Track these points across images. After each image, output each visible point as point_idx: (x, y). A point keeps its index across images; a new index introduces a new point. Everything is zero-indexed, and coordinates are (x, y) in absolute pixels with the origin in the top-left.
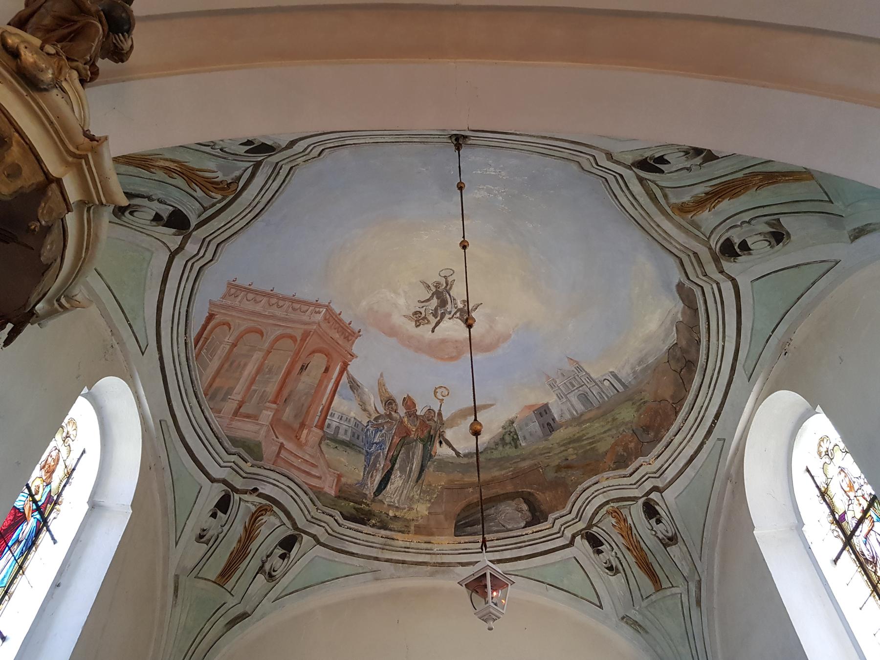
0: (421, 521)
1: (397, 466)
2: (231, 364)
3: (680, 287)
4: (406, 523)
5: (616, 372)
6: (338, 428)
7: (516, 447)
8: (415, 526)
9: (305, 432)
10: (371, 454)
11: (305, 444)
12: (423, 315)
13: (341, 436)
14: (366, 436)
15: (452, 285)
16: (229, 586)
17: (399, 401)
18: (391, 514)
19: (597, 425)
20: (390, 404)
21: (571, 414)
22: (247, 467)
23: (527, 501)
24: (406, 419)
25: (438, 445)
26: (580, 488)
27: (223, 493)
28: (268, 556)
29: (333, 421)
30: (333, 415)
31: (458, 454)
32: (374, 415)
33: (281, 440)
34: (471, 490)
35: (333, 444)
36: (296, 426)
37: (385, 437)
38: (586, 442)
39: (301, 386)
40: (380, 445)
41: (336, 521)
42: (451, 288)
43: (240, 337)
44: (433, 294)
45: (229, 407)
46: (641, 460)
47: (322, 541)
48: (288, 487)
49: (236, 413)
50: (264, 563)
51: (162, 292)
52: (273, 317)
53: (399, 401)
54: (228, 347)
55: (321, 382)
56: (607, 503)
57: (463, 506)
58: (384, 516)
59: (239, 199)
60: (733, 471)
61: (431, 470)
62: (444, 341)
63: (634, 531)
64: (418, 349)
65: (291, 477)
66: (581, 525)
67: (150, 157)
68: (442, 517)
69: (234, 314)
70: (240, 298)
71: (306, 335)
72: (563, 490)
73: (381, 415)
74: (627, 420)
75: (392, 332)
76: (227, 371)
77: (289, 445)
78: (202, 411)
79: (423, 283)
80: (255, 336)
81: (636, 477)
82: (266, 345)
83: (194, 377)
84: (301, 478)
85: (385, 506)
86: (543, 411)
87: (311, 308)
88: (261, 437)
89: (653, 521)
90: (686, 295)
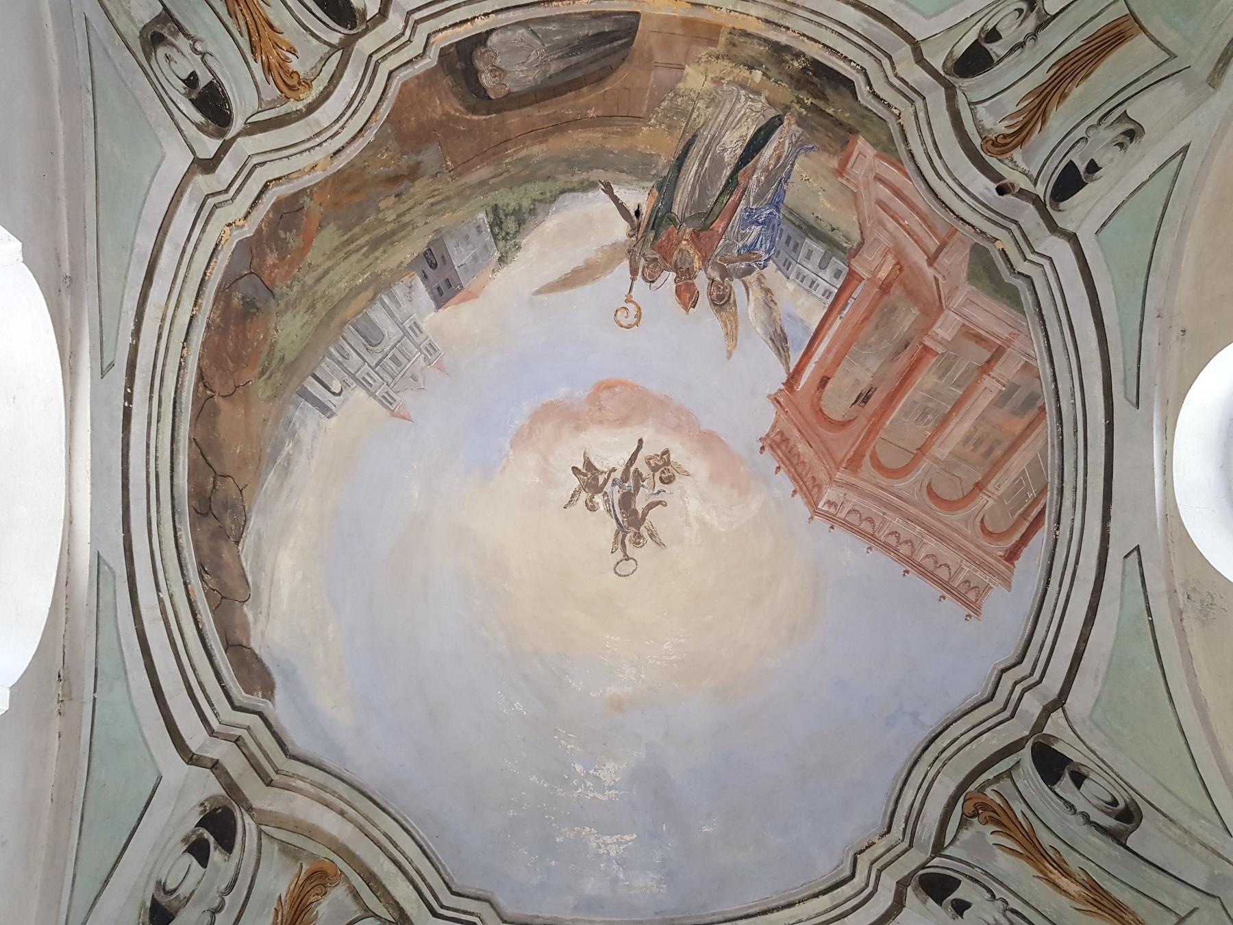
0: (703, 52)
1: (727, 172)
2: (991, 450)
3: (268, 690)
4: (734, 51)
5: (324, 420)
6: (822, 267)
7: (495, 208)
8: (714, 42)
9: (882, 275)
10: (770, 204)
11: (887, 251)
12: (658, 475)
13: (819, 249)
14: (773, 241)
15: (615, 542)
16: (1120, 10)
17: (704, 301)
18: (758, 75)
19: (342, 285)
20: (720, 298)
21: (393, 298)
22: (1005, 241)
23: (481, 92)
24: (697, 264)
25: (645, 211)
26: (370, 136)
27: (1062, 205)
28: (1021, 45)
29: (828, 281)
30: (827, 293)
31: (608, 190)
32: (751, 279)
33: (930, 272)
34: (591, 113)
35: (837, 236)
36: (896, 291)
37: (738, 233)
38: (362, 241)
39: (874, 364)
40: (751, 219)
41: (869, 83)
42: (617, 534)
43: (968, 498)
44: (643, 519)
45: (1007, 370)
46: (248, 231)
47: (907, 48)
48: (941, 178)
49: (998, 353)
50: (1034, 35)
51: (1084, 639)
52: (909, 518)
53: (704, 301)
54: (990, 487)
55: (837, 363)
56: (311, 108)
57: (611, 79)
58: (774, 73)
59: (960, 778)
60: (67, 302)
61: (663, 160)
62: (623, 421)
63: (244, 43)
64: (664, 403)
65: (931, 197)
66: (366, 45)
67: (1090, 908)
68: (659, 58)
69: (972, 548)
70: (961, 577)
71: (854, 464)
72: (407, 130)
73: (739, 277)
74: (288, 316)
75: (708, 441)
76: (999, 442)
77: (919, 258)
78: (1055, 380)
79: (660, 544)
80: (942, 490)
81: (254, 187)
82: (925, 464)
83: (1057, 453)
84: (913, 188)
85: (766, 93)
86: (445, 292)
87: (842, 515)
88: (966, 289)
89: (204, 79)
90: (253, 672)
